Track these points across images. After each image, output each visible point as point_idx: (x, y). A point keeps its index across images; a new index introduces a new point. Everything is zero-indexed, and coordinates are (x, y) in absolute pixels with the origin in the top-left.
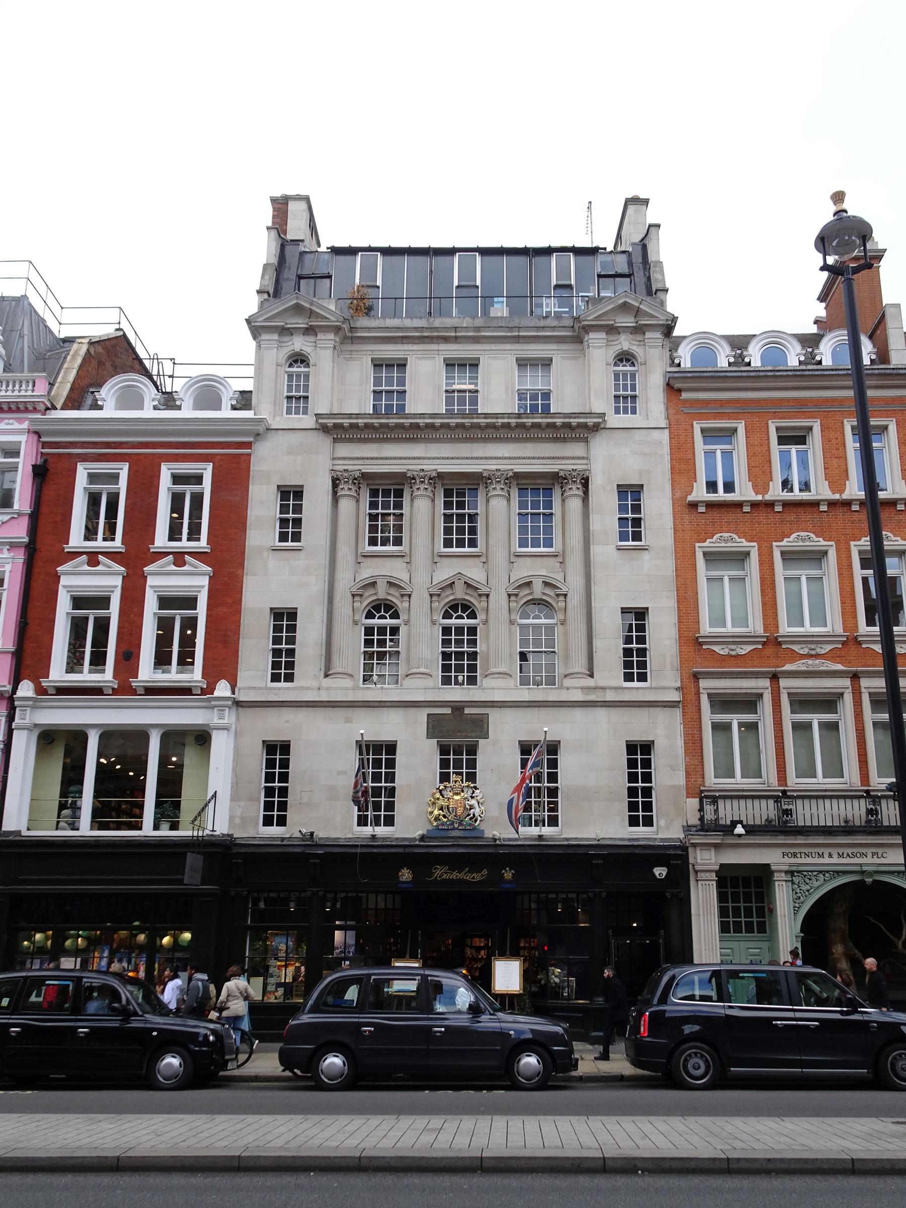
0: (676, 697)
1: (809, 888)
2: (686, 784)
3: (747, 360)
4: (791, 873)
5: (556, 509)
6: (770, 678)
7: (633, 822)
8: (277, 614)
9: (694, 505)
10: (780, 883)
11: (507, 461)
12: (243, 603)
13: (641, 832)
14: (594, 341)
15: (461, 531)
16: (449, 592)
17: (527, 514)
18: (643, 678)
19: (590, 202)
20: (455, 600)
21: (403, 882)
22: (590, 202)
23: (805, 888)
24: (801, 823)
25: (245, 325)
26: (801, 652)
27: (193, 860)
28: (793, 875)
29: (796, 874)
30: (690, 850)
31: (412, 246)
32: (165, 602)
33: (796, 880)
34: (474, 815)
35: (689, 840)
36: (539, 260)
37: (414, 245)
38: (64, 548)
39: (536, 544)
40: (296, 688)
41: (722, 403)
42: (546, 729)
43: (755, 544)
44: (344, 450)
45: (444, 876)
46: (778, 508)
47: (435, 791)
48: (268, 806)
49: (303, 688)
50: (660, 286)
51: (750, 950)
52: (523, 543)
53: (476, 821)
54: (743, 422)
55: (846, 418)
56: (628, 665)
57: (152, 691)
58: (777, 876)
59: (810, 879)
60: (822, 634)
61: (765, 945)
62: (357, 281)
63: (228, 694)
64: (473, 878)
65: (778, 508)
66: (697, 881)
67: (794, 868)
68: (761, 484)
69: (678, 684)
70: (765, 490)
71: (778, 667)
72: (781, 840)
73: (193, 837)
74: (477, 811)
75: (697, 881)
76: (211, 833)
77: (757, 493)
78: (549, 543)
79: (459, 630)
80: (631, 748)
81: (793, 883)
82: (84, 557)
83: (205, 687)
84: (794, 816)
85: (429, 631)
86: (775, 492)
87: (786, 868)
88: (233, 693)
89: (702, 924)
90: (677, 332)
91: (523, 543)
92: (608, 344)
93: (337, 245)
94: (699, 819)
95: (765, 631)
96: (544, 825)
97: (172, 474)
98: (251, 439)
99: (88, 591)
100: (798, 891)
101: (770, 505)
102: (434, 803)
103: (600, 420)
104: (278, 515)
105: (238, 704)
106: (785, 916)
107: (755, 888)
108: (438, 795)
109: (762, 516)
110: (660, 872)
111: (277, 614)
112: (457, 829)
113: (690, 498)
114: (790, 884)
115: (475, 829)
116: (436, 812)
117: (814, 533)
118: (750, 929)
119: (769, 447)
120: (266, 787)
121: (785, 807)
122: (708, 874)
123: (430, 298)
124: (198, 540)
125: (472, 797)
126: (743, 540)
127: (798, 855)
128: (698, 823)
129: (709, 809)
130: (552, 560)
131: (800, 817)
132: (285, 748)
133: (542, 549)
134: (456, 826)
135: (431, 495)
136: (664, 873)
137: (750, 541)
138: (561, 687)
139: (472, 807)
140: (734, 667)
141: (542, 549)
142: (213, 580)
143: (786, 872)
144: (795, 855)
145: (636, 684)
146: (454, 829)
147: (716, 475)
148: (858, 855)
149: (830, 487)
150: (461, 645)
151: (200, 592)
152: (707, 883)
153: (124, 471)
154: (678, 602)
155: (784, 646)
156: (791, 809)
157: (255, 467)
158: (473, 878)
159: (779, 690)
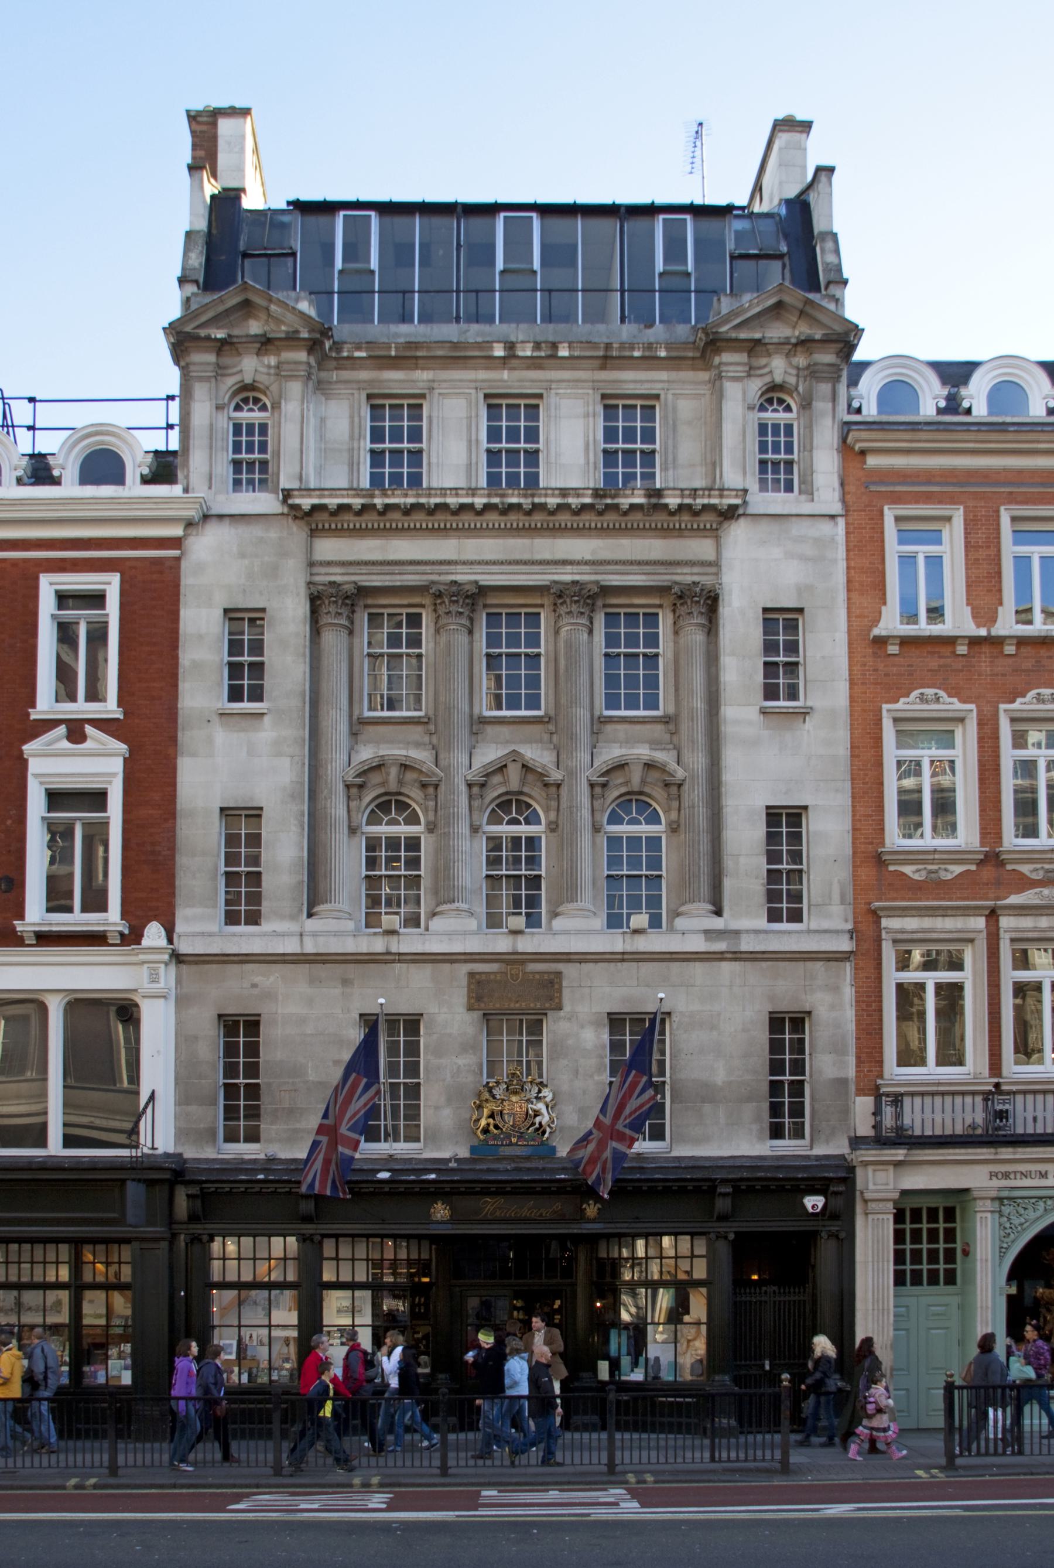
0: (845, 945)
1: (1023, 1220)
2: (856, 1077)
3: (966, 404)
4: (1001, 1200)
5: (665, 647)
6: (986, 916)
7: (776, 1132)
8: (773, 815)
9: (881, 642)
10: (984, 1215)
11: (586, 568)
12: (178, 801)
13: (787, 1147)
14: (731, 368)
15: (632, 681)
16: (497, 779)
17: (619, 655)
18: (796, 916)
19: (701, 124)
20: (507, 793)
21: (438, 1222)
22: (701, 124)
23: (1016, 1221)
24: (1020, 1130)
25: (162, 332)
26: (1034, 876)
27: (134, 1191)
28: (1002, 1204)
29: (1006, 1202)
30: (859, 1172)
31: (394, 200)
32: (56, 798)
33: (1006, 1210)
34: (540, 1123)
35: (857, 1157)
36: (639, 224)
37: (431, 198)
38: (28, 714)
39: (632, 704)
40: (264, 935)
41: (928, 476)
42: (661, 995)
43: (972, 706)
44: (329, 548)
45: (498, 1214)
46: (1010, 649)
47: (482, 1088)
48: (231, 1113)
49: (275, 934)
50: (832, 276)
51: (933, 1308)
52: (612, 702)
53: (544, 1133)
54: (962, 508)
55: (1004, 504)
56: (773, 896)
57: (45, 938)
58: (980, 1205)
59: (1025, 1209)
60: (953, 849)
61: (955, 1301)
62: (660, 266)
63: (163, 942)
64: (541, 1215)
65: (1010, 649)
66: (867, 1214)
67: (1005, 1194)
68: (985, 614)
69: (849, 926)
70: (993, 620)
71: (998, 898)
72: (985, 1153)
73: (131, 1157)
74: (545, 1119)
75: (867, 1214)
76: (150, 1152)
77: (978, 626)
78: (533, 702)
79: (393, 843)
80: (776, 1022)
81: (1001, 1216)
82: (62, 729)
83: (126, 932)
84: (1011, 1121)
85: (468, 843)
86: (1006, 625)
87: (994, 1194)
88: (170, 941)
89: (870, 1273)
90: (858, 356)
91: (612, 702)
92: (751, 371)
93: (305, 197)
94: (874, 1127)
95: (982, 844)
96: (644, 1140)
97: (57, 592)
98: (177, 531)
99: (75, 782)
100: (1008, 1225)
101: (996, 642)
102: (479, 1107)
103: (738, 501)
104: (226, 659)
105: (178, 958)
106: (986, 1260)
107: (945, 1222)
108: (486, 1095)
109: (984, 663)
110: (813, 1202)
111: (773, 815)
112: (516, 1144)
113: (876, 632)
114: (997, 1215)
115: (542, 1143)
116: (483, 1122)
117: (945, 690)
118: (933, 1280)
119: (999, 551)
120: (225, 1085)
121: (999, 1107)
122: (881, 1205)
123: (458, 291)
124: (103, 700)
125: (538, 1098)
126: (955, 700)
127: (1012, 1176)
128: (871, 1133)
129: (888, 1111)
130: (420, 729)
131: (1020, 1122)
132: (253, 1025)
133: (642, 713)
134: (514, 1140)
135: (468, 623)
136: (820, 1205)
137: (965, 702)
138: (671, 929)
139: (537, 1114)
140: (934, 899)
141: (642, 713)
142: (129, 765)
143: (993, 1199)
144: (1006, 1175)
145: (785, 926)
146: (511, 1144)
147: (1031, 599)
148: (1000, 1176)
149: (974, 617)
150: (498, 867)
151: (110, 783)
152: (881, 1216)
153: (112, 585)
154: (853, 797)
155: (1009, 867)
156: (1007, 1111)
157: (188, 580)
158: (541, 1215)
159: (998, 935)
